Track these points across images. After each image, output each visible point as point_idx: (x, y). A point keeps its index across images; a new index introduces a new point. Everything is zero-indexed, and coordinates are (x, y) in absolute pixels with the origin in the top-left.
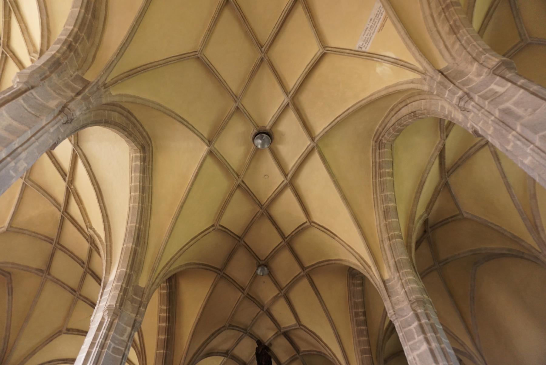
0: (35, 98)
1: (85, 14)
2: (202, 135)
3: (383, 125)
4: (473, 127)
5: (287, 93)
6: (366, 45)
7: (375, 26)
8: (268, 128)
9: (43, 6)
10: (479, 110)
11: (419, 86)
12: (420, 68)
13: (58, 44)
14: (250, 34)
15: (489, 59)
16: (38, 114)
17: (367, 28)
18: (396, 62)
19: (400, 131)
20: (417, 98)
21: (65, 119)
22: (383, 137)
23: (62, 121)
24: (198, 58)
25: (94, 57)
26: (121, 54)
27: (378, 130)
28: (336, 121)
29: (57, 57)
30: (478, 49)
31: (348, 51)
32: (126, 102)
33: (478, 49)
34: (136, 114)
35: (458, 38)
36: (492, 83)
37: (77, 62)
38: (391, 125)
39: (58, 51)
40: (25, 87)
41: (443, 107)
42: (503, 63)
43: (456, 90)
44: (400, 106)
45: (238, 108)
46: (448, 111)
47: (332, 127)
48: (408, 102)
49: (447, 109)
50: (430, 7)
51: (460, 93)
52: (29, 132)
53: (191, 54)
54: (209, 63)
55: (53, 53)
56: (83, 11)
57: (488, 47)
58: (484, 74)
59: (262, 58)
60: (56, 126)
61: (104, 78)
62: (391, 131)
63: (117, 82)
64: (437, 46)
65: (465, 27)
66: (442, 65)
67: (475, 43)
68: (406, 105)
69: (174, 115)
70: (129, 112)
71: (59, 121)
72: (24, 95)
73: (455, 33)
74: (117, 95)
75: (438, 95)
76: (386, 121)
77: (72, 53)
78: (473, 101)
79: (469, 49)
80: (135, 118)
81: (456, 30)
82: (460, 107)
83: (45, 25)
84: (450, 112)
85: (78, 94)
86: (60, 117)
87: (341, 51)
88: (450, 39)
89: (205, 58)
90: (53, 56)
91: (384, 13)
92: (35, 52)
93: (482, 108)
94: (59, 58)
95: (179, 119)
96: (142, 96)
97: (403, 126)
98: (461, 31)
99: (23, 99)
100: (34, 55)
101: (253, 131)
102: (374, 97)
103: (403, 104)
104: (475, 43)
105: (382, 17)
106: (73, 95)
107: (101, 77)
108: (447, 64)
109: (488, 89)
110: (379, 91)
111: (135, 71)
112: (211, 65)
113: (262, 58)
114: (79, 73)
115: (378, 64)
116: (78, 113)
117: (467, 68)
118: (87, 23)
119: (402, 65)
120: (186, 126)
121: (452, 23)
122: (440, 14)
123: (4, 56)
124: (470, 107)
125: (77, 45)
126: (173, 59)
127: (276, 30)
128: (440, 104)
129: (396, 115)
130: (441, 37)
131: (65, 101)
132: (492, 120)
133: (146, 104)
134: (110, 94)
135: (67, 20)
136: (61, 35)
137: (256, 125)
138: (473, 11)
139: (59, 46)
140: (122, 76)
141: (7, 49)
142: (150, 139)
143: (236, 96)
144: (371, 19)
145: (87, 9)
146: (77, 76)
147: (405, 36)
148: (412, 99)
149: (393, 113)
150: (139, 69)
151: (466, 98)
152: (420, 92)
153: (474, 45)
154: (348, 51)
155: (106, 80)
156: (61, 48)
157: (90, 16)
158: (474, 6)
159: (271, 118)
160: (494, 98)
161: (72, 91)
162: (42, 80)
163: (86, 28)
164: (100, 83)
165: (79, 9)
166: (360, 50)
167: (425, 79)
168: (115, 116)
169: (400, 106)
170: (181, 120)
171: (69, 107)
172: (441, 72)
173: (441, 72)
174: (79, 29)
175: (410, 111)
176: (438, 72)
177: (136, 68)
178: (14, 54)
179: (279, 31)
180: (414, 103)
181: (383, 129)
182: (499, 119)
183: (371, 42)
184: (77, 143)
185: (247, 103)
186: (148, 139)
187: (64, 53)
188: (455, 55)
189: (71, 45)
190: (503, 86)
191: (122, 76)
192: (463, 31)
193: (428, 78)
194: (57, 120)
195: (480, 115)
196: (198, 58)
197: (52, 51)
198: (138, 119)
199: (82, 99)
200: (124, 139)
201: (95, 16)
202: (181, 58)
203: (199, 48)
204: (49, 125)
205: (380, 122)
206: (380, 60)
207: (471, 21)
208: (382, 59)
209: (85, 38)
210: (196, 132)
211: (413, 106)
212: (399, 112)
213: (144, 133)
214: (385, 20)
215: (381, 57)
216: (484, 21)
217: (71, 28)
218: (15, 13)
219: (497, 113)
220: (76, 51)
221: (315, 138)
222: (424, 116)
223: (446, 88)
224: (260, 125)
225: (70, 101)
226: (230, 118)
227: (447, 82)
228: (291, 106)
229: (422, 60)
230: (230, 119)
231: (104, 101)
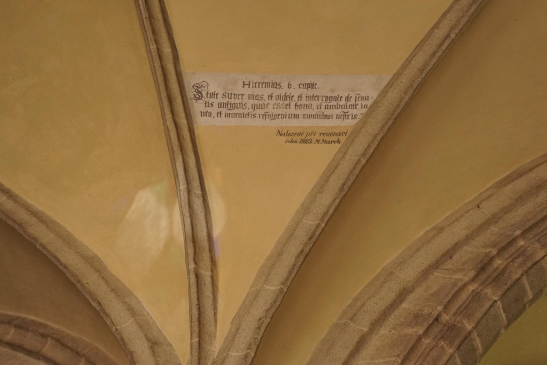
6: (214, 110)
7: (292, 110)
17: (276, 85)
18: (200, 249)
31: (167, 50)
50: (425, 274)
91: (350, 123)
102: (37, 230)
110: (69, 241)
121: (521, 243)
122: (416, 318)
144: (311, 86)
147: (302, 236)
154: (167, 50)
166: (190, 93)
183: (234, 122)
206: (183, 187)
208: (189, 191)
212: (20, 355)
214: (328, 137)
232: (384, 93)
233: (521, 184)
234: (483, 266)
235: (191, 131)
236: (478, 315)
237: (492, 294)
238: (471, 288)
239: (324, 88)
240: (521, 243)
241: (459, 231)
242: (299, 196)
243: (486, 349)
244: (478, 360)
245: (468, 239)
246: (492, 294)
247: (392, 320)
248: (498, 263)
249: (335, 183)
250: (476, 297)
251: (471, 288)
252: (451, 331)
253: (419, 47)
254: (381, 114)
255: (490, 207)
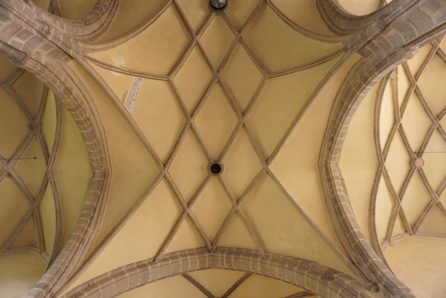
0: (405, 37)
1: (349, 104)
2: (272, 8)
3: (112, 14)
4: (30, 6)
5: (198, 44)
6: (136, 81)
7: (131, 95)
8: (214, 14)
9: (377, 110)
10: (29, 21)
11: (87, 46)
12: (89, 61)
13: (374, 82)
14: (227, 91)
15: (33, 67)
16: (407, 22)
17: (137, 94)
18: (110, 67)
19: (96, 8)
20: (86, 37)
21: (386, 19)
22: (111, 4)
23: (389, 17)
24: (268, 73)
25: (349, 73)
26: (328, 75)
27: (116, 10)
28: (154, 18)
29: (378, 72)
30: (45, 75)
31: (150, 77)
32: (332, 37)
33: (45, 75)
34: (325, 27)
35: (64, 84)
36: (25, 46)
37: (363, 69)
38: (105, 14)
39: (376, 76)
40: (410, 47)
41: (62, 27)
42: (20, 62)
43: (54, 40)
44: (100, 31)
45: (240, 32)
46: (56, 24)
47: (157, 13)
48: (93, 35)
49: (58, 25)
50: (90, 108)
51: (50, 37)
52: (420, 5)
53: (274, 76)
54: (260, 69)
55: (380, 75)
56: (349, 107)
57: (37, 76)
58: (34, 54)
59: (218, 73)
60: (395, 12)
61: (346, 56)
62: (103, 8)
63: (336, 53)
64: (79, 79)
65: (60, 93)
66: (71, 63)
67: (49, 80)
68: (95, 31)
69: (294, 26)
70: (331, 29)
71: (392, 16)
72: (413, 39)
73: (67, 88)
74: (338, 42)
75: (70, 38)
76: (110, 18)
77: (365, 75)
78: (36, 30)
79: (53, 75)
80: (327, 24)
81: (66, 90)
82: (47, 24)
83: (379, 98)
84: (54, 22)
85: (370, 42)
86: (390, 20)
87: (156, 77)
88: (69, 83)
89: (263, 73)
90: (380, 72)
91: (125, 105)
92: (392, 80)
93: (26, 23)
94: (376, 71)
95: (290, 23)
96: (318, 42)
97: (95, 12)
98: (63, 90)
99: (415, 35)
100: (394, 77)
101: (227, 11)
102: (124, 39)
103: (97, 32)
104: (49, 80)
105: (126, 102)
106: (374, 41)
107: (347, 57)
108: (68, 64)
109: (27, 40)
110: (120, 44)
111: (319, 63)
112: (259, 67)
113: (218, 73)
114: (364, 60)
115: (125, 66)
116: (374, 25)
117: (50, 60)
118: (348, 98)
119: (105, 64)
120: (284, 16)
121: (71, 97)
122: (82, 103)
123: (416, 78)
124: (37, 24)
125: (360, 82)
126: (289, 72)
127: (207, 94)
128: (65, 31)
129: (102, 23)
130: (77, 86)
131: (382, 35)
132: (15, 10)
133: (316, 36)
134: (343, 43)
135: (362, 100)
136: (369, 89)
137: (224, 16)
138: (57, 106)
139: (374, 81)
140: (331, 58)
141: (412, 83)
142: (317, 5)
143: (240, 42)
144: (134, 100)
145: (346, 107)
146: (366, 57)
147: (106, 87)
148: (90, 36)
149: (105, 25)
150: (316, 64)
151: (44, 33)
152: (85, 42)
153: (49, 78)
154: (150, 77)
155: (345, 54)
156: (373, 79)
157: (345, 103)
158: (57, 110)
159: (211, 23)
160: (18, 32)
161: (374, 44)
162: (395, 52)
163: (350, 94)
164: (349, 52)
165: (352, 108)
166: (140, 78)
167: (83, 52)
168: (343, 25)
169: (100, 31)
170: (288, 22)
171: (380, 30)
172: (72, 58)
173: (72, 58)
174: (355, 93)
175: (90, 26)
176: (74, 57)
177: (319, 64)
178: (408, 78)
179: (205, 93)
180: (88, 33)
181: (111, 10)
182: (7, 9)
183: (132, 84)
184: (381, 3)
185: (231, 36)
186: (319, 5)
187: (371, 75)
188: (62, 71)
189: (366, 80)
190: (13, 42)
191: (331, 58)
192: (61, 90)
193: (81, 53)
194: (393, 18)
195: (27, 16)
196: (269, 73)
197: (380, 77)
198: (324, 24)
199: (368, 37)
200: (340, 5)
201: (342, 103)
202: (282, 73)
203: (268, 81)
204: (401, 12)
205: (115, 17)
206: (123, 69)
207: (55, 96)
208: (122, 70)
209: (352, 87)
210: (276, 11)
211: (89, 30)
212: (100, 25)
213: (321, 10)
214: (124, 100)
215: (123, 72)
216: (47, 96)
217: (361, 94)
218: (398, 107)
219: (12, 16)
220: (362, 76)
221: (172, 4)
222: (78, 21)
223: (63, 43)
224: (220, 16)
225: (378, 35)
226: (246, 23)
227: (64, 48)
228: (194, 33)
229: (89, 68)
230: (247, 22)
231: (350, 37)
232: (128, 113)
233: (103, 132)
234: (88, 119)
235: (133, 75)
236: (79, 115)
237: (82, 119)
238: (85, 116)
239: (133, 102)
240: (91, 128)
241: (97, 118)
242: (114, 90)
243: (71, 114)
244: (353, 216)
245: (95, 119)
246: (82, 119)
247: (83, 98)
248: (88, 122)
249: (114, 97)
250: (83, 116)
251: (85, 116)
252: (77, 109)
253: (135, 122)
254: (125, 111)
255: (100, 125)
